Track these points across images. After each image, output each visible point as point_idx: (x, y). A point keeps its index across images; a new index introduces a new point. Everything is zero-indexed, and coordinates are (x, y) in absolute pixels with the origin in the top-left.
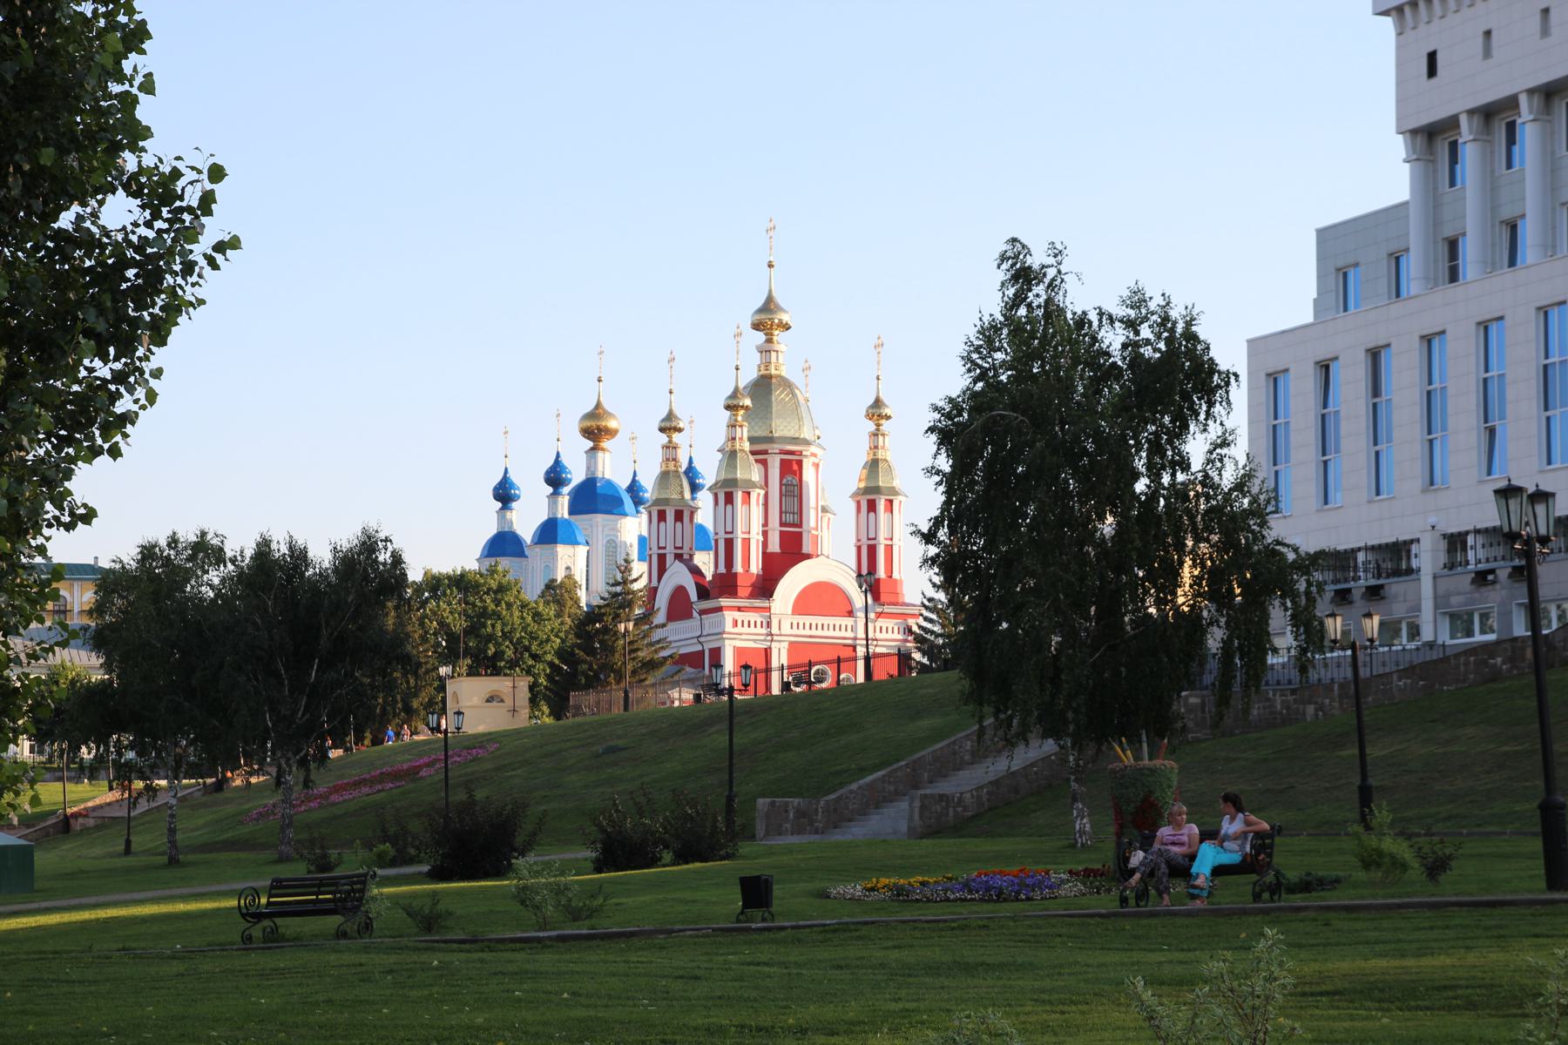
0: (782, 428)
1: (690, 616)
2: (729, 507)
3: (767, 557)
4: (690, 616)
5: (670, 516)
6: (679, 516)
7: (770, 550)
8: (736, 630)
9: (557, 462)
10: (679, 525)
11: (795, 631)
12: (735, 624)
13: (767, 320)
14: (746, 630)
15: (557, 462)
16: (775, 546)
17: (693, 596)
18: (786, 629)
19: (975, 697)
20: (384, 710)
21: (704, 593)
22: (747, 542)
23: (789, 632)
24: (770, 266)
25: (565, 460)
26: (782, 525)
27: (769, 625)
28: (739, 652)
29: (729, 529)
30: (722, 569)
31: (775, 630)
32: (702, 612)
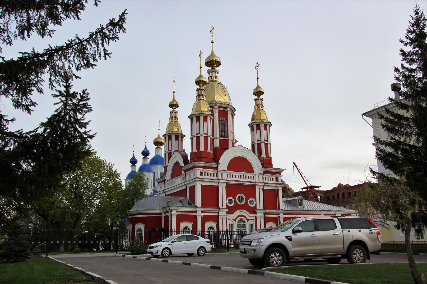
0: (220, 98)
1: (181, 174)
2: (198, 123)
3: (215, 149)
4: (181, 174)
5: (173, 138)
6: (177, 138)
7: (215, 146)
8: (201, 177)
9: (146, 148)
10: (177, 141)
11: (229, 178)
12: (201, 174)
13: (212, 63)
14: (206, 177)
15: (146, 148)
16: (217, 145)
17: (182, 164)
18: (225, 177)
19: (409, 184)
20: (419, 276)
21: (186, 162)
22: (206, 138)
23: (226, 178)
24: (212, 42)
25: (148, 149)
26: (220, 136)
27: (217, 175)
28: (203, 187)
29: (198, 132)
30: (195, 150)
31: (220, 177)
32: (185, 171)
